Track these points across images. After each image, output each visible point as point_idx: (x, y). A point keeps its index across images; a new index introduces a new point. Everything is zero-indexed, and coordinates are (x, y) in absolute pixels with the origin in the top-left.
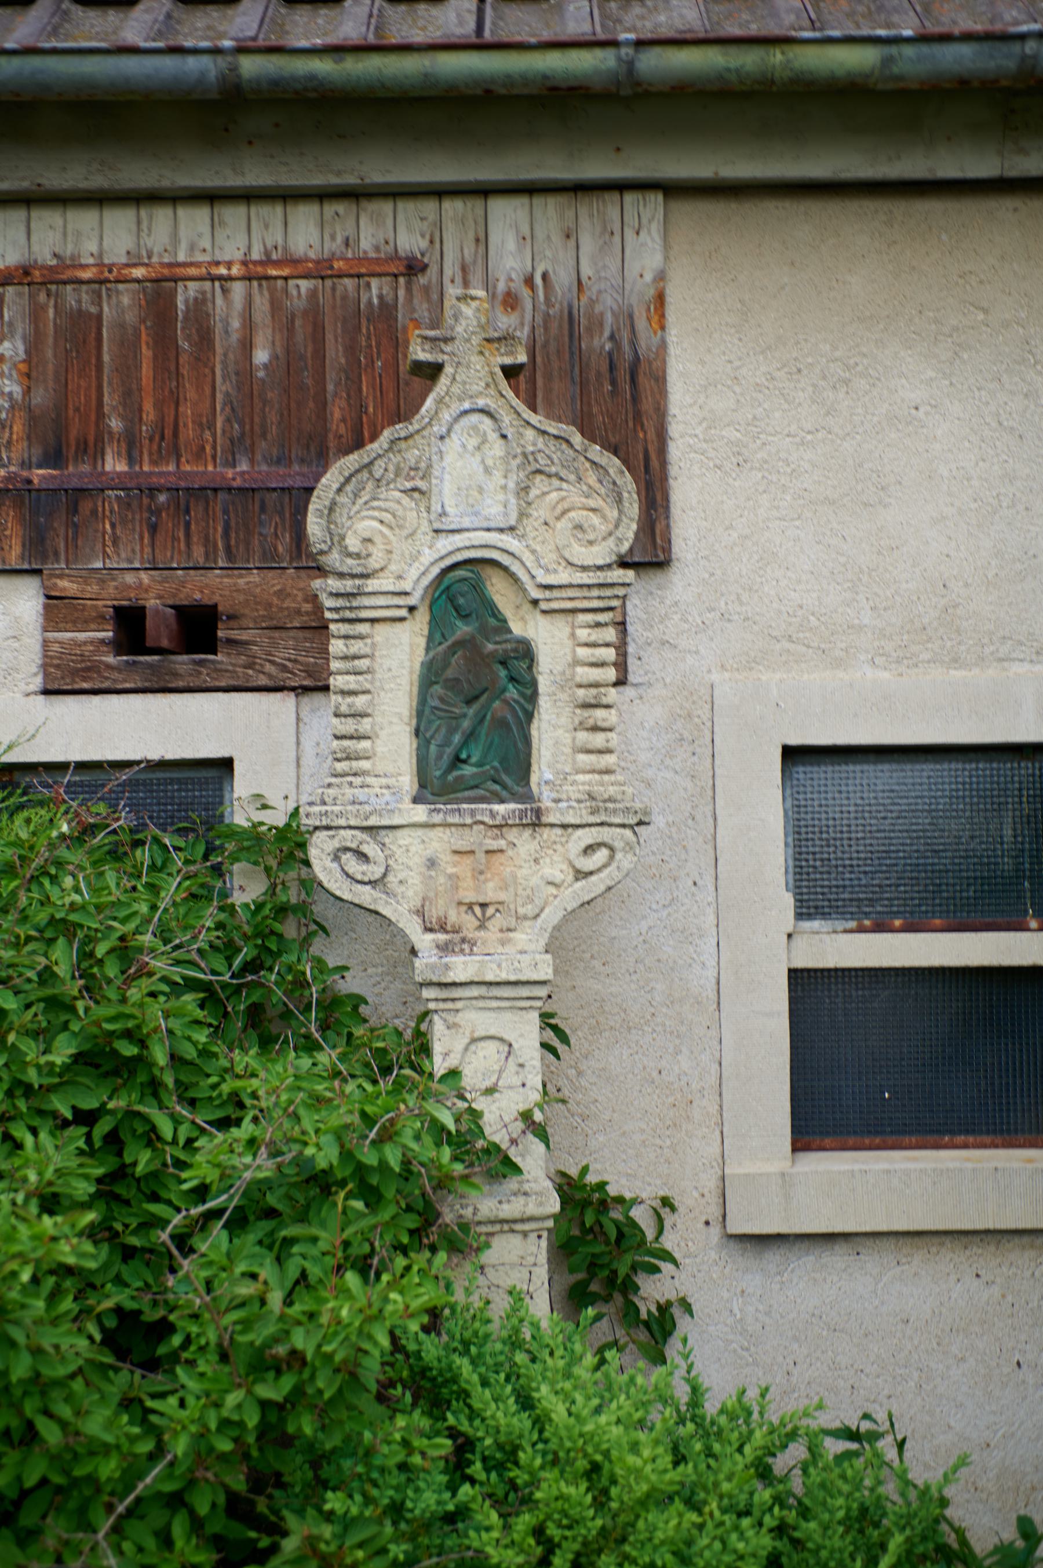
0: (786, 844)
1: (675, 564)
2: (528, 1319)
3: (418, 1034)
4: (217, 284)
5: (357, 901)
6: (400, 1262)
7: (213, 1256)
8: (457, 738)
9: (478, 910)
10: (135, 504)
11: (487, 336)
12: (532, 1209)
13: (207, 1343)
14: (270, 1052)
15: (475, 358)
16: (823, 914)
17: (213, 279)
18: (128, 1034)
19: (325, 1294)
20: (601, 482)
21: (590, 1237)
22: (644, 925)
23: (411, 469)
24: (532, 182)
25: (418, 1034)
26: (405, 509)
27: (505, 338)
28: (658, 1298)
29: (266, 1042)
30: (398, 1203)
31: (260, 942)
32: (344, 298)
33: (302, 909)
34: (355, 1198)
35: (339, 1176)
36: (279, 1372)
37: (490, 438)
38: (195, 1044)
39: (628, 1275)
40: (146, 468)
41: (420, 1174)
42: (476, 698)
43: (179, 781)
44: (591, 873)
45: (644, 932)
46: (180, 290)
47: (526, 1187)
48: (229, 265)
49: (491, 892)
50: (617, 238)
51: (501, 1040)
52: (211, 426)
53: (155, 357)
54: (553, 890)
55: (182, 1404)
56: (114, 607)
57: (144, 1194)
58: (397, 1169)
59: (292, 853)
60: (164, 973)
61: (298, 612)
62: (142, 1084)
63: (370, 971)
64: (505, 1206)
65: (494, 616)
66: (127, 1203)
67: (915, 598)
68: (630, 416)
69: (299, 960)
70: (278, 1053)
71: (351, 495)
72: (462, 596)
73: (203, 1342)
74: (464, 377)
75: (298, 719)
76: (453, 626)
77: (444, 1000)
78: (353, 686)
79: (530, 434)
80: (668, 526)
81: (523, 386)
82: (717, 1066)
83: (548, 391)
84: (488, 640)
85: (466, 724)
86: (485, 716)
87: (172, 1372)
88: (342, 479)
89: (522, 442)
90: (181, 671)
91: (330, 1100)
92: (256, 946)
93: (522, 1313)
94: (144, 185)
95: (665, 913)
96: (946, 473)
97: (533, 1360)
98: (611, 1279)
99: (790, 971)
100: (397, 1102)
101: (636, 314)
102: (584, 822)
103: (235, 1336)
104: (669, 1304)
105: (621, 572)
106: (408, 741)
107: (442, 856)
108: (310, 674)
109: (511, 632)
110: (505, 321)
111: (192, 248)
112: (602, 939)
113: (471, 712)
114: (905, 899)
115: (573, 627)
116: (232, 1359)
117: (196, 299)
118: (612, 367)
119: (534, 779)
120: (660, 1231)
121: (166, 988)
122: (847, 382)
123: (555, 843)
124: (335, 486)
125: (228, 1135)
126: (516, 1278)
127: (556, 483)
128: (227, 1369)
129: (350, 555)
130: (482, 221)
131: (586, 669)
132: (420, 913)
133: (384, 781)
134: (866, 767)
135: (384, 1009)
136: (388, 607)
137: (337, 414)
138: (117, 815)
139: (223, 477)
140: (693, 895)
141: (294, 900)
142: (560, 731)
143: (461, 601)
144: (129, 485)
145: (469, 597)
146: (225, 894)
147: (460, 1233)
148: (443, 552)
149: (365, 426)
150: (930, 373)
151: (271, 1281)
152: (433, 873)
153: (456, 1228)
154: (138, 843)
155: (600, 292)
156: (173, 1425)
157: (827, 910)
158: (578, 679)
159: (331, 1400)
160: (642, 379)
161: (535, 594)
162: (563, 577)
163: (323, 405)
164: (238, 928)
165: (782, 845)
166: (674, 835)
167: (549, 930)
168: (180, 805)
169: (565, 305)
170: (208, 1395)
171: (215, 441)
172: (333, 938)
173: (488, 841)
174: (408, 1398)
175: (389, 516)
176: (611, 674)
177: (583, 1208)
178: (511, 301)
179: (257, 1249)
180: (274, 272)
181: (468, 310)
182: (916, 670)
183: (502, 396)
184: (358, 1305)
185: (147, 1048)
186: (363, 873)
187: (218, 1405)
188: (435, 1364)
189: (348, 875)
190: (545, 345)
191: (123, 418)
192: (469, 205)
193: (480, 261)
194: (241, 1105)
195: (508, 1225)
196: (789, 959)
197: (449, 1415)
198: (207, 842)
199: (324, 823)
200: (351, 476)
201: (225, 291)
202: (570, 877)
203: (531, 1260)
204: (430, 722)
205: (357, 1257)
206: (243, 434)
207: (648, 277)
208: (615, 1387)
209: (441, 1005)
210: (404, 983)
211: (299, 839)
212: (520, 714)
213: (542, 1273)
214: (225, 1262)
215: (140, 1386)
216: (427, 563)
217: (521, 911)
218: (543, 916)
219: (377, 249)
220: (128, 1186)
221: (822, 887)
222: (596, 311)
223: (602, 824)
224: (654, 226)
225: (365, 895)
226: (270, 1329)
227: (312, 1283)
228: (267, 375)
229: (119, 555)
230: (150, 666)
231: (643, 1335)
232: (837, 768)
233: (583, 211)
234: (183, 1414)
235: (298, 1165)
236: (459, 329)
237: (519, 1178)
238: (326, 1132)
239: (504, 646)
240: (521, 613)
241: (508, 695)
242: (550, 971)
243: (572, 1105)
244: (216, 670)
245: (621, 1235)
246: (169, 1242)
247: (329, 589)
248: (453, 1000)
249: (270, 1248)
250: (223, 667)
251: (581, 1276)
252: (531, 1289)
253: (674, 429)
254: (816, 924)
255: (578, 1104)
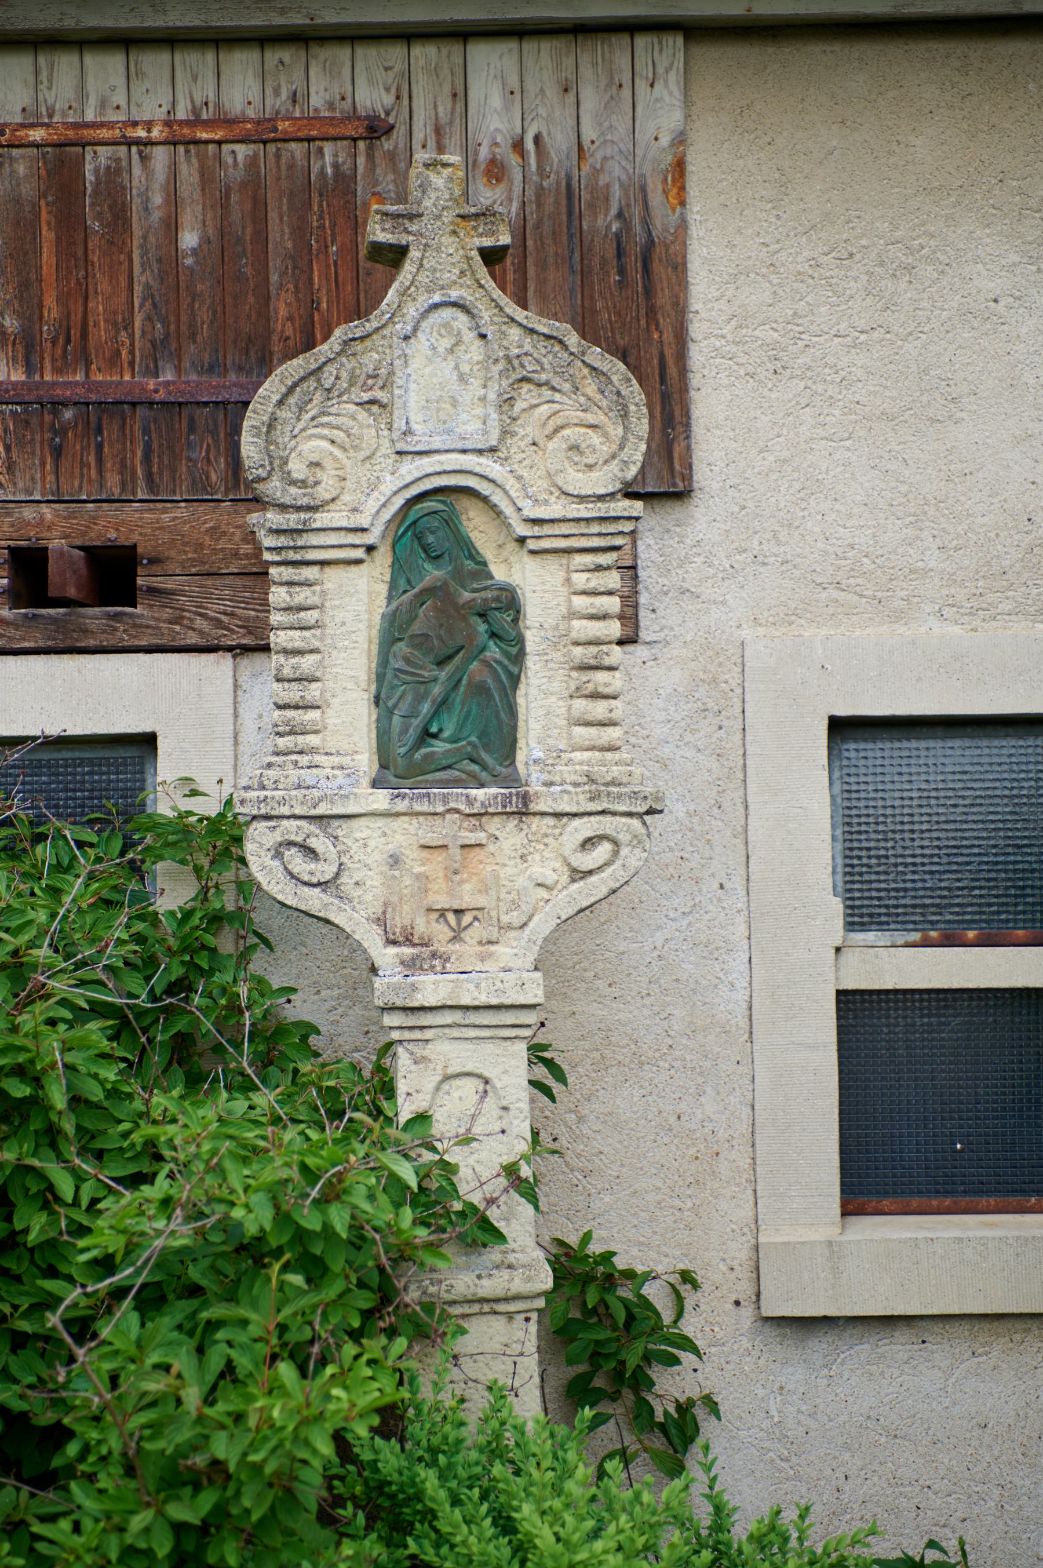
0: (834, 838)
1: (696, 493)
2: (511, 1421)
3: (380, 1069)
4: (134, 149)
5: (303, 908)
6: (350, 1349)
7: (118, 1344)
8: (426, 708)
9: (451, 917)
10: (34, 421)
11: (462, 212)
12: (518, 1286)
13: (110, 1453)
14: (198, 1093)
15: (447, 240)
16: (880, 923)
17: (129, 143)
18: (20, 1071)
19: (253, 1390)
20: (602, 392)
21: (594, 1320)
22: (659, 938)
23: (369, 377)
24: (522, 22)
25: (380, 1069)
26: (361, 426)
27: (484, 214)
28: (677, 1395)
29: (194, 1081)
30: (347, 1277)
31: (187, 958)
32: (291, 167)
33: (240, 916)
34: (295, 1272)
35: (274, 1244)
36: (197, 1487)
37: (465, 338)
38: (102, 1082)
39: (638, 1366)
40: (48, 378)
41: (374, 1241)
42: (450, 657)
43: (91, 762)
44: (590, 872)
45: (659, 945)
46: (88, 157)
47: (511, 1258)
48: (149, 125)
49: (467, 897)
50: (626, 92)
51: (479, 1076)
52: (128, 325)
53: (58, 240)
54: (543, 894)
55: (77, 1528)
56: (9, 548)
57: (38, 1267)
58: (344, 1236)
59: (227, 849)
60: (64, 995)
61: (236, 554)
62: (36, 1132)
63: (323, 993)
64: (485, 1282)
65: (471, 557)
66: (18, 1279)
67: (992, 535)
68: (643, 312)
69: (235, 981)
70: (207, 1093)
71: (294, 409)
72: (432, 533)
73: (104, 1451)
74: (433, 263)
75: (236, 686)
76: (420, 570)
77: (411, 1028)
78: (298, 644)
79: (515, 332)
80: (688, 448)
81: (510, 277)
82: (749, 1110)
83: (541, 282)
84: (463, 587)
85: (437, 690)
86: (460, 680)
87: (66, 1489)
88: (284, 390)
89: (505, 343)
90: (92, 627)
91: (267, 1151)
92: (183, 963)
93: (504, 1414)
94: (43, 25)
95: (685, 923)
96: (1032, 381)
97: (517, 1473)
98: (618, 1374)
99: (839, 993)
100: (346, 1153)
101: (650, 186)
102: (582, 810)
103: (142, 1444)
104: (691, 1403)
105: (627, 503)
106: (366, 711)
107: (407, 852)
108: (250, 631)
109: (492, 578)
110: (487, 195)
111: (103, 104)
112: (608, 954)
113: (443, 675)
114: (980, 905)
115: (568, 571)
116: (139, 1472)
117: (108, 168)
118: (620, 253)
119: (521, 757)
120: (680, 1314)
121: (68, 1015)
122: (909, 268)
123: (546, 835)
124: (276, 398)
125: (137, 1194)
126: (498, 1371)
127: (547, 394)
128: (133, 1484)
129: (293, 483)
130: (459, 71)
131: (585, 622)
132: (381, 921)
133: (336, 760)
134: (931, 743)
135: (341, 1040)
136: (340, 546)
137: (283, 312)
138: (9, 802)
139: (143, 389)
140: (719, 900)
141: (230, 907)
142: (553, 699)
143: (431, 539)
144: (27, 399)
145: (440, 534)
146: (141, 898)
147: (422, 1314)
148: (409, 479)
149: (317, 326)
150: (1015, 258)
151: (186, 1375)
152: (397, 873)
153: (418, 1308)
154: (40, 838)
155: (605, 159)
156: (65, 1555)
157: (884, 919)
158: (574, 635)
159: (262, 1522)
160: (657, 267)
161: (522, 530)
162: (556, 509)
163: (265, 300)
164: (162, 941)
165: (829, 838)
166: (697, 828)
167: (539, 942)
168: (91, 791)
169: (563, 174)
170: (109, 1518)
171: (132, 344)
172: (278, 950)
173: (464, 834)
174: (361, 1519)
175: (342, 434)
176: (614, 629)
177: (585, 1284)
178: (496, 171)
179: (175, 1334)
180: (205, 136)
181: (438, 180)
182: (994, 623)
183: (481, 286)
184: (293, 1404)
185: (42, 1087)
186: (311, 873)
187: (122, 1530)
188: (395, 1477)
189: (292, 876)
190: (538, 226)
191: (19, 315)
192: (445, 51)
193: (458, 121)
194: (159, 1158)
195: (489, 1304)
196: (837, 979)
197: (410, 1540)
198: (125, 837)
199: (263, 811)
200: (295, 385)
201: (144, 159)
202: (565, 878)
203: (517, 1348)
204: (393, 688)
205: (297, 1344)
206: (167, 336)
207: (665, 140)
208: (617, 1507)
209: (407, 1035)
210: (366, 1008)
211: (236, 832)
212: (503, 677)
213: (530, 1365)
214: (133, 1351)
215: (26, 1508)
216: (389, 493)
217: (505, 919)
218: (531, 925)
219: (331, 106)
220: (19, 1258)
221: (878, 890)
222: (601, 183)
223: (603, 812)
224: (672, 76)
225: (314, 900)
226: (185, 1435)
227: (240, 1377)
228: (197, 262)
229: (15, 484)
230: (54, 620)
231: (658, 1442)
232: (897, 745)
233: (585, 59)
234: (78, 1541)
235: (224, 1231)
236: (427, 203)
237: (503, 1247)
238: (257, 1191)
239: (483, 594)
240: (505, 553)
241: (488, 654)
242: (540, 992)
243: (569, 1155)
244: (135, 626)
245: (631, 1318)
246: (60, 1327)
247: (268, 525)
248: (422, 1028)
249: (191, 1334)
250: (144, 622)
251: (582, 1368)
252: (516, 1384)
253: (696, 329)
254: (870, 937)
255: (579, 1156)
